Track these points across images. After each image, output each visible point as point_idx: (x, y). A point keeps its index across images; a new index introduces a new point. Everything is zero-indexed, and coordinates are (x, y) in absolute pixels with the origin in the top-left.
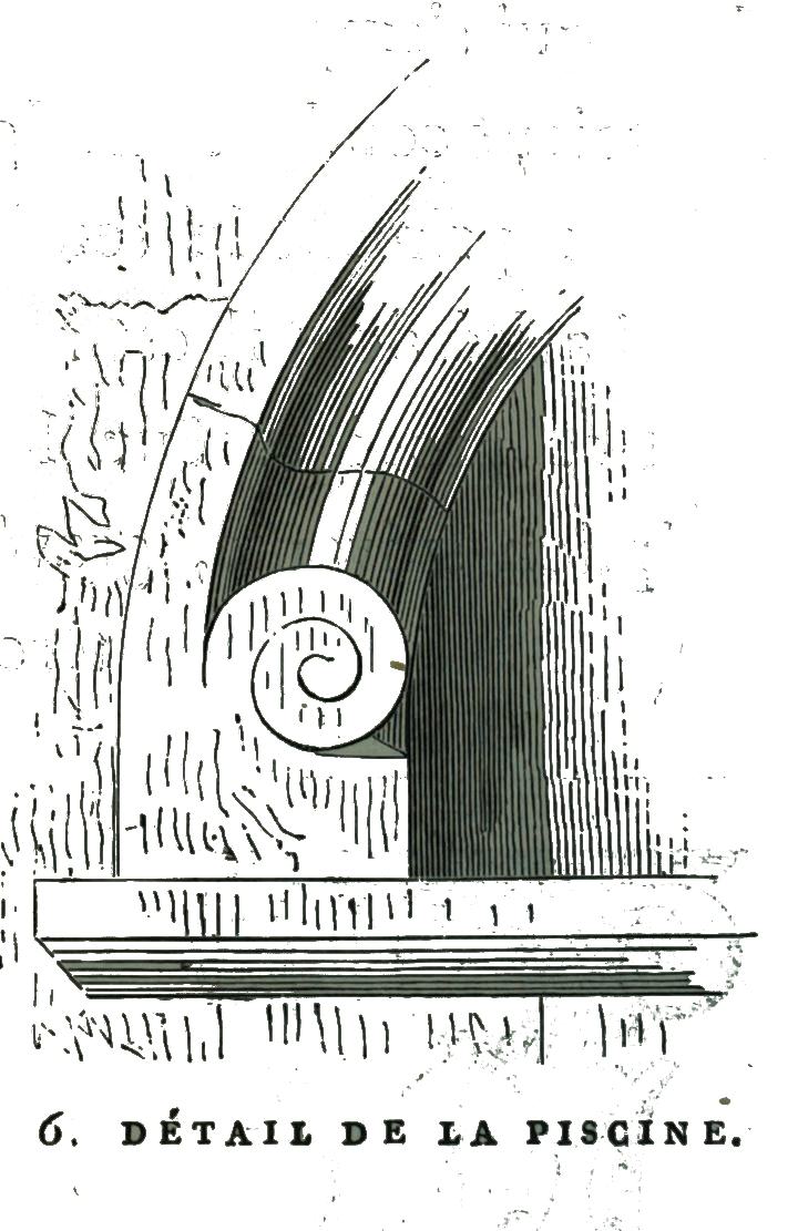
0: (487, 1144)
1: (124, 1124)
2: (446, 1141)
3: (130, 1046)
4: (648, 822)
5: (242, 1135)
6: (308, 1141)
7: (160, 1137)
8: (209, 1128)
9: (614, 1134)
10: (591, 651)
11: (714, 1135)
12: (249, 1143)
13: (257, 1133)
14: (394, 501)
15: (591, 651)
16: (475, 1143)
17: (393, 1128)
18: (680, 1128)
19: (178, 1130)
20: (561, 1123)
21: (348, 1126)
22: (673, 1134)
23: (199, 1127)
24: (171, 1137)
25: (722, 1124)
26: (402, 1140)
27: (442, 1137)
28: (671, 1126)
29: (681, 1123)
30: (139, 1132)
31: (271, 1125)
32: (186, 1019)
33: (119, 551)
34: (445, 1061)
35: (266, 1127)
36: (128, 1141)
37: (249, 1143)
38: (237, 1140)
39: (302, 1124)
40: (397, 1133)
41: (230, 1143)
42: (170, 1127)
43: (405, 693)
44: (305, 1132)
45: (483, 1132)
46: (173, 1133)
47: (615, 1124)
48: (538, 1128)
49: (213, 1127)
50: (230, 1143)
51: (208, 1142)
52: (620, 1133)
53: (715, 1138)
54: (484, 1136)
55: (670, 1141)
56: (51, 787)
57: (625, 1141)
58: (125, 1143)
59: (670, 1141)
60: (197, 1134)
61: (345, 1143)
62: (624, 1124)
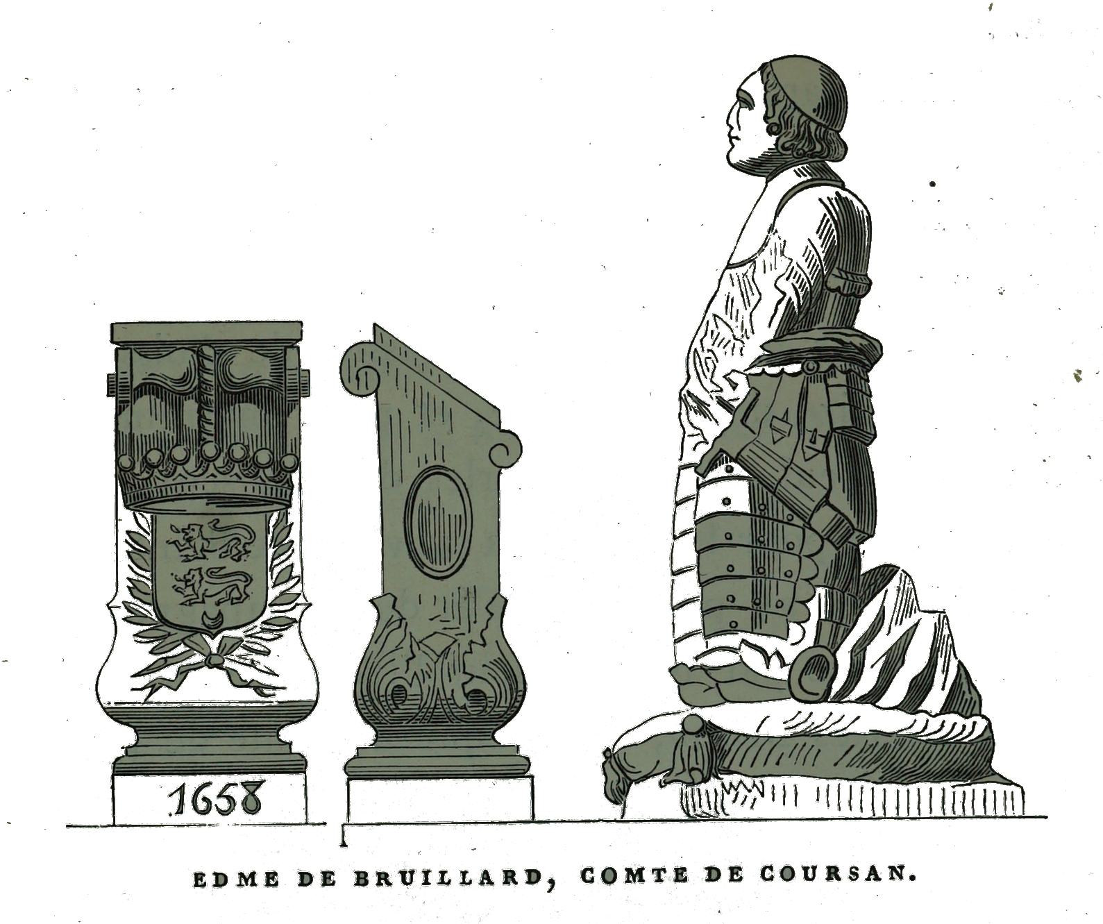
3: (727, 817)
5: (488, 878)
8: (662, 873)
10: (766, 622)
11: (199, 881)
12: (880, 879)
13: (497, 877)
15: (766, 622)
17: (735, 871)
18: (899, 870)
19: (332, 877)
21: (710, 869)
22: (894, 874)
23: (655, 872)
25: (204, 875)
26: (276, 884)
27: (462, 881)
28: (892, 868)
30: (612, 872)
32: (1046, 817)
34: (170, 815)
36: (709, 879)
37: (880, 879)
38: (872, 877)
40: (737, 875)
41: (868, 879)
43: (839, 641)
44: (247, 874)
45: (485, 876)
46: (201, 880)
47: (586, 870)
49: (665, 872)
50: (868, 879)
51: (662, 881)
52: (768, 873)
53: (272, 882)
57: (592, 881)
60: (654, 876)
61: (300, 885)
62: (771, 868)
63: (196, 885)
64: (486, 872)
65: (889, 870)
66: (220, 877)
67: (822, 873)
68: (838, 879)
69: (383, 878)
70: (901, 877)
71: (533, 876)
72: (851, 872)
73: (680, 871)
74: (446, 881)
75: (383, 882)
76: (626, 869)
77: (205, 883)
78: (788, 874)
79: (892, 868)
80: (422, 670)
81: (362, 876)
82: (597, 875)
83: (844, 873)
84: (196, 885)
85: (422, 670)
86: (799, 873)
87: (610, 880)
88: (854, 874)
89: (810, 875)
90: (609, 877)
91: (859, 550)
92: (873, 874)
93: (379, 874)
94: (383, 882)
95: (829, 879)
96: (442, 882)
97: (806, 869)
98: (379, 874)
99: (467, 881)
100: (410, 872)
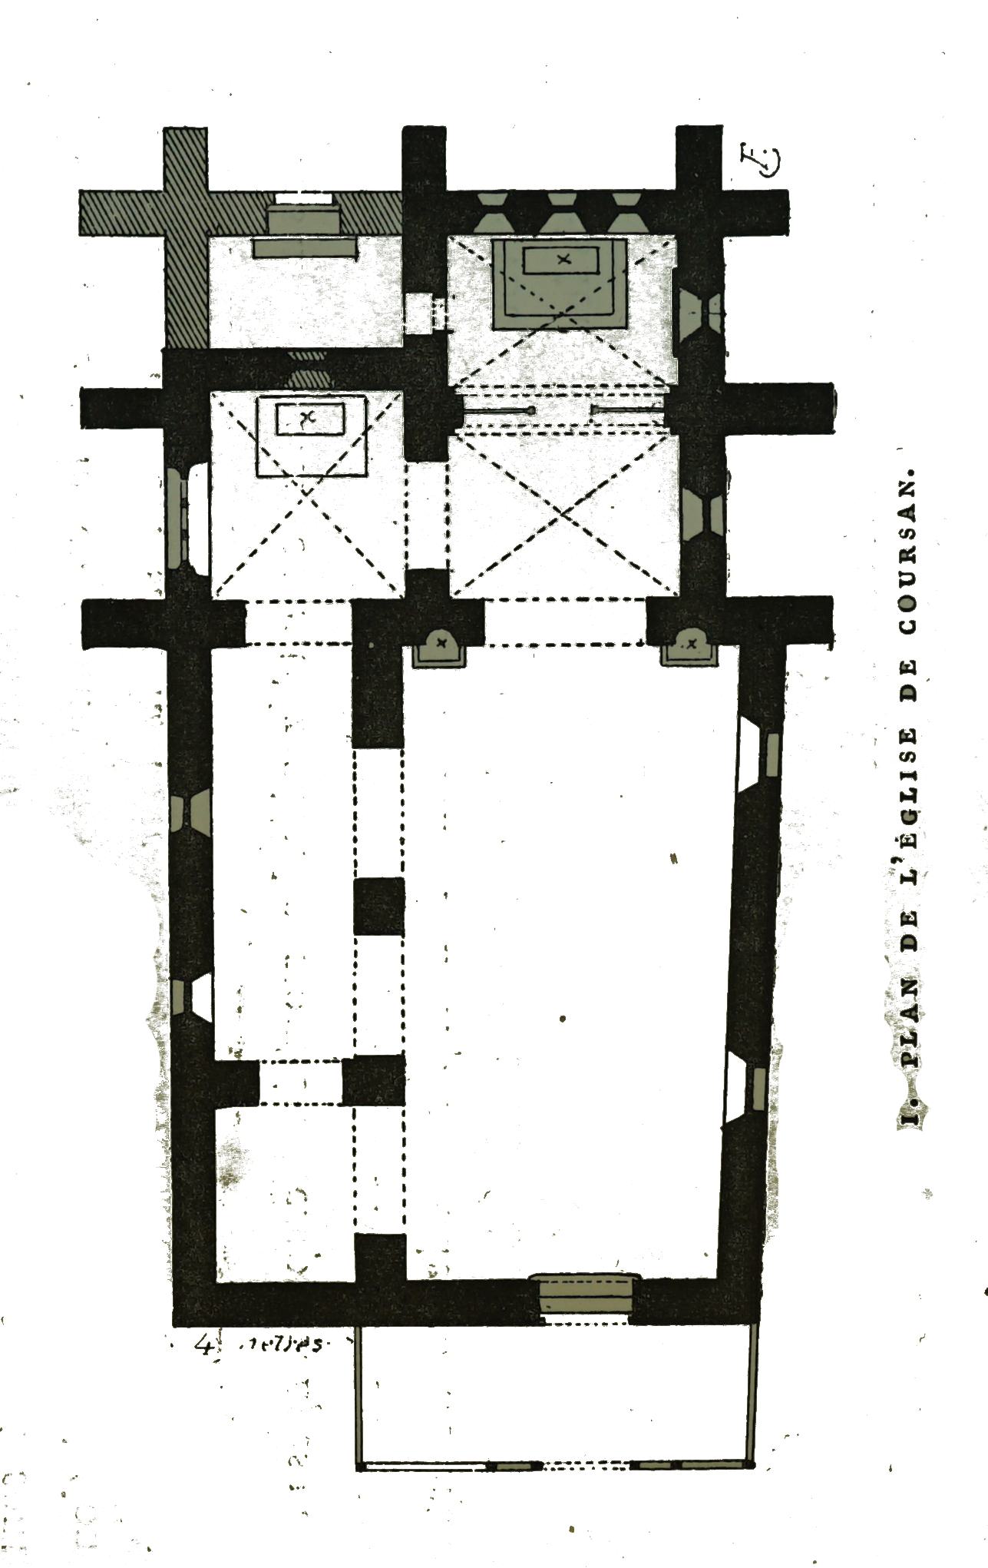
0: (914, 511)
1: (901, 700)
2: (914, 880)
4: (618, 1282)
5: (910, 1010)
6: (914, 872)
7: (912, 926)
9: (909, 581)
11: (910, 919)
13: (909, 1001)
14: (184, 162)
16: (913, 519)
17: (907, 919)
18: (907, 985)
19: (905, 663)
20: (902, 882)
21: (902, 697)
24: (911, 668)
25: (902, 663)
26: (914, 913)
28: (902, 493)
29: (900, 485)
31: (903, 776)
33: (198, 1344)
35: (905, 779)
36: (913, 697)
37: (913, 506)
39: (902, 794)
40: (909, 734)
41: (913, 519)
42: (904, 841)
48: (906, 1059)
52: (908, 626)
53: (912, 840)
54: (908, 513)
55: (912, 494)
56: (596, 291)
58: (915, 884)
59: (912, 494)
61: (915, 700)
63: (914, 845)
64: (900, 513)
65: (904, 496)
66: (904, 693)
67: (907, 566)
68: (913, 549)
69: (907, 556)
70: (911, 484)
71: (905, 490)
72: (906, 760)
73: (903, 737)
74: (910, 875)
75: (911, 555)
76: (903, 995)
77: (912, 835)
78: (908, 604)
79: (902, 493)
80: (291, 1337)
81: (904, 556)
82: (907, 617)
83: (907, 544)
84: (914, 845)
85: (291, 1337)
86: (907, 590)
87: (912, 602)
88: (909, 534)
89: (908, 578)
90: (908, 604)
91: (197, 833)
92: (908, 513)
93: (901, 560)
94: (911, 555)
95: (913, 559)
96: (913, 798)
97: (902, 584)
98: (901, 560)
99: (911, 1037)
100: (900, 576)
